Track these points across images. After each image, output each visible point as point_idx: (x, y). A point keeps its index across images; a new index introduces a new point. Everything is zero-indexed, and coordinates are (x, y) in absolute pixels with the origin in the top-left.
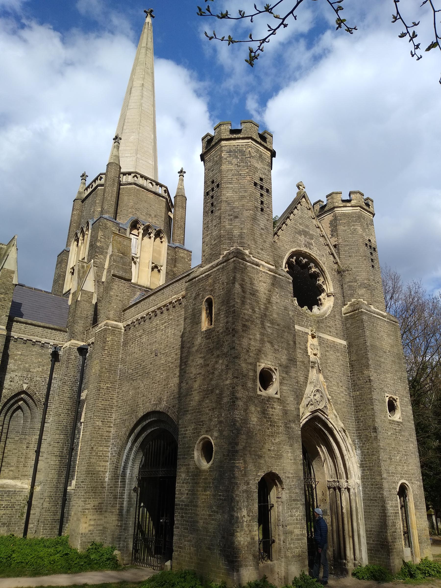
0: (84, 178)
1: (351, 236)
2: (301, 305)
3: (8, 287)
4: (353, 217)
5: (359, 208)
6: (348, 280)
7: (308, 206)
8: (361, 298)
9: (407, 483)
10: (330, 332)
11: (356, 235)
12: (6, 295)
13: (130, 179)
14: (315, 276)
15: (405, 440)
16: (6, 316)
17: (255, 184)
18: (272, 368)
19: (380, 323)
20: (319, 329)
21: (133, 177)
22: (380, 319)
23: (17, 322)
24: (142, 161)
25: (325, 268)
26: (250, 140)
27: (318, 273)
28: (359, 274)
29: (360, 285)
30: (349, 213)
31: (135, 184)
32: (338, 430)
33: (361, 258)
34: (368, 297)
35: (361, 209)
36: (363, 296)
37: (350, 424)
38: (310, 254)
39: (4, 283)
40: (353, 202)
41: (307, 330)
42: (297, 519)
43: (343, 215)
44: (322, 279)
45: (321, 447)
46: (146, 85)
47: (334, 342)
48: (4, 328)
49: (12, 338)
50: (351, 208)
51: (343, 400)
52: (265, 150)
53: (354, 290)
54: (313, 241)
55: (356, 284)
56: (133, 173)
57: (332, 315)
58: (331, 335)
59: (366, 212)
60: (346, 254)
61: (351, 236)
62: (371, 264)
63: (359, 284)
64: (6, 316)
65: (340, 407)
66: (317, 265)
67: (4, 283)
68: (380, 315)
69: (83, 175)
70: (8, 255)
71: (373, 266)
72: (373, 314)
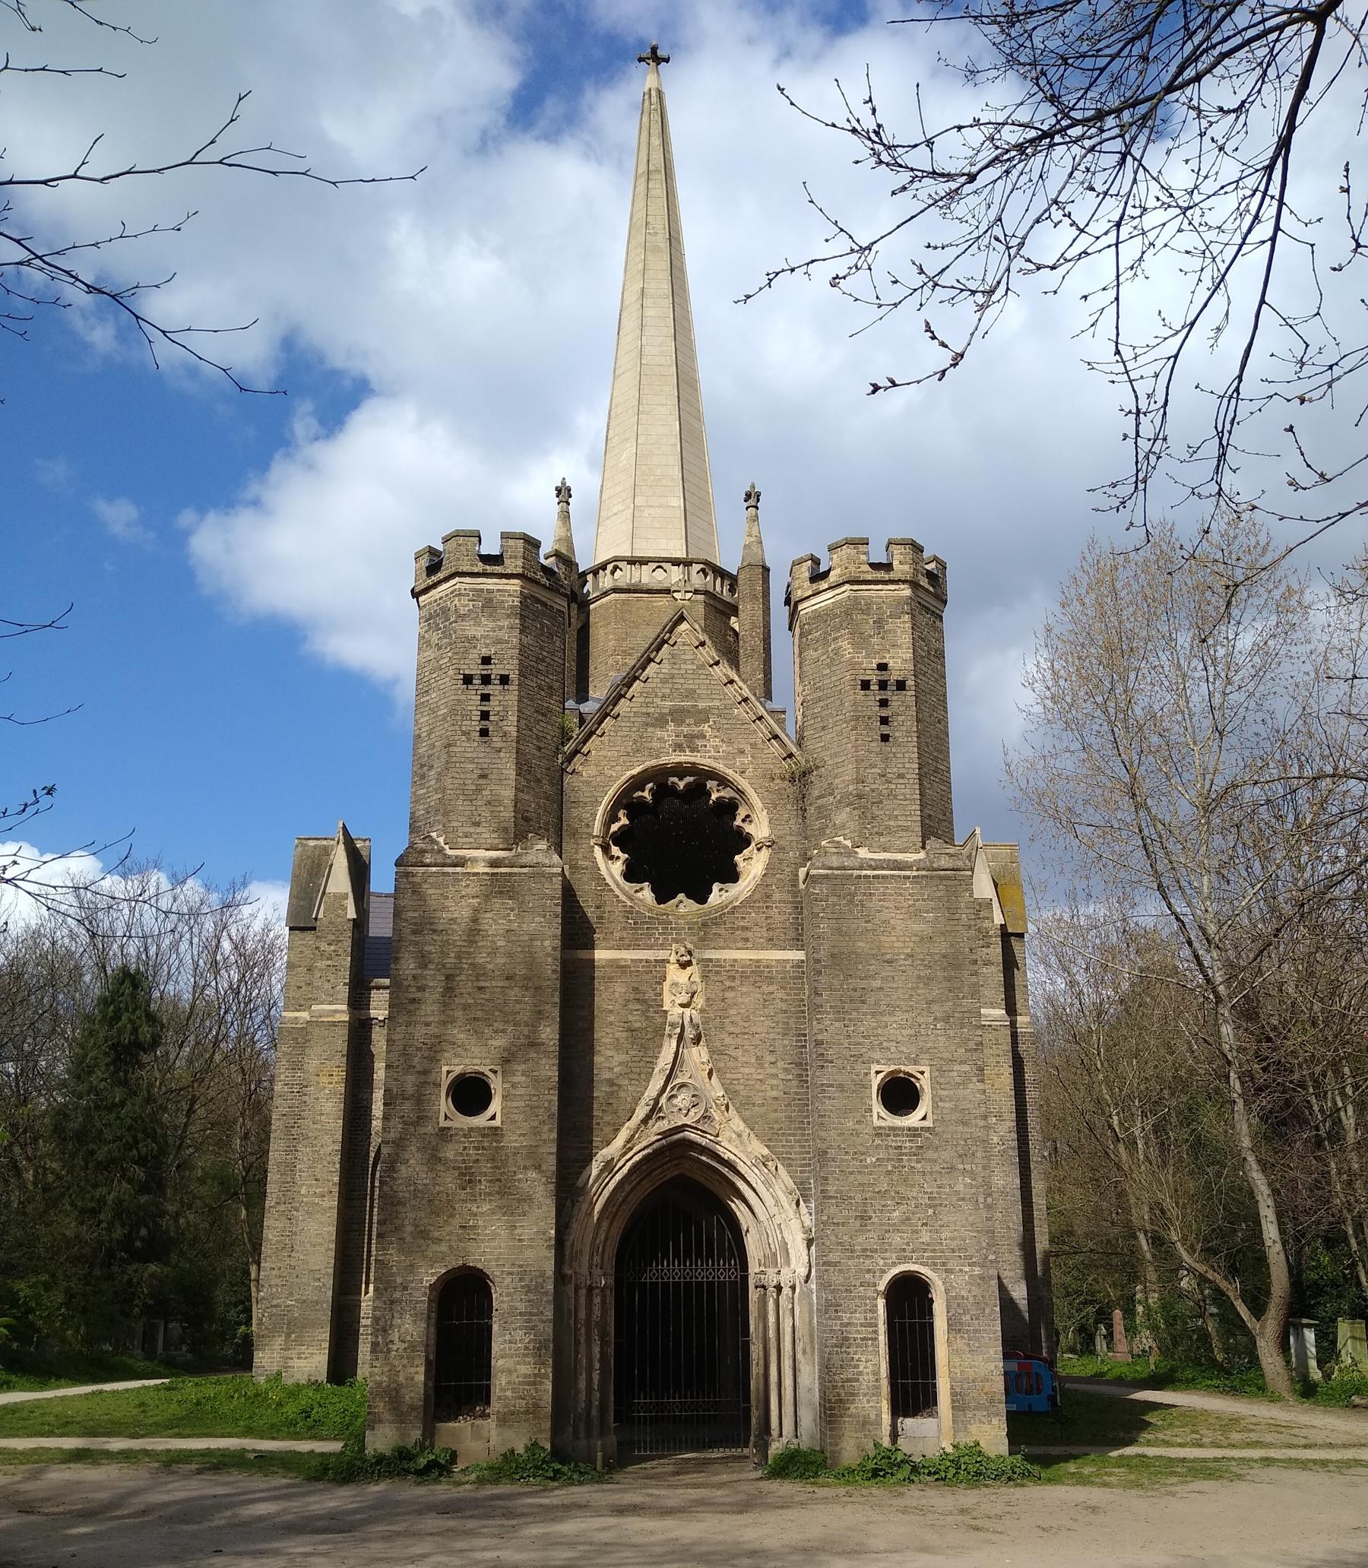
0: (752, 502)
1: (828, 671)
2: (663, 895)
3: (341, 928)
4: (835, 616)
5: (847, 587)
6: (816, 793)
7: (697, 638)
8: (840, 833)
9: (925, 1271)
10: (746, 940)
11: (839, 667)
12: (340, 944)
13: (606, 581)
14: (729, 808)
15: (937, 1168)
16: (345, 984)
17: (468, 680)
18: (485, 1069)
19: (879, 888)
20: (704, 942)
21: (613, 573)
22: (884, 877)
23: (378, 988)
24: (651, 511)
25: (743, 783)
26: (457, 579)
27: (732, 799)
28: (840, 770)
29: (840, 802)
30: (827, 608)
31: (615, 590)
32: (749, 1164)
33: (845, 725)
34: (852, 828)
35: (856, 587)
36: (843, 827)
37: (792, 1147)
38: (694, 763)
39: (331, 923)
40: (833, 577)
41: (662, 954)
42: (526, 1348)
43: (814, 618)
44: (742, 812)
45: (733, 1201)
46: (650, 290)
47: (758, 961)
48: (344, 1007)
49: (374, 1022)
50: (830, 594)
51: (774, 1093)
52: (504, 581)
53: (827, 817)
54: (706, 727)
55: (831, 799)
56: (608, 562)
57: (758, 896)
58: (747, 949)
59: (880, 587)
60: (815, 726)
61: (828, 671)
62: (878, 729)
63: (838, 797)
64: (345, 984)
65: (763, 1110)
66: (724, 782)
67: (331, 923)
68: (883, 868)
69: (748, 496)
70: (331, 865)
71: (885, 738)
72: (856, 873)
